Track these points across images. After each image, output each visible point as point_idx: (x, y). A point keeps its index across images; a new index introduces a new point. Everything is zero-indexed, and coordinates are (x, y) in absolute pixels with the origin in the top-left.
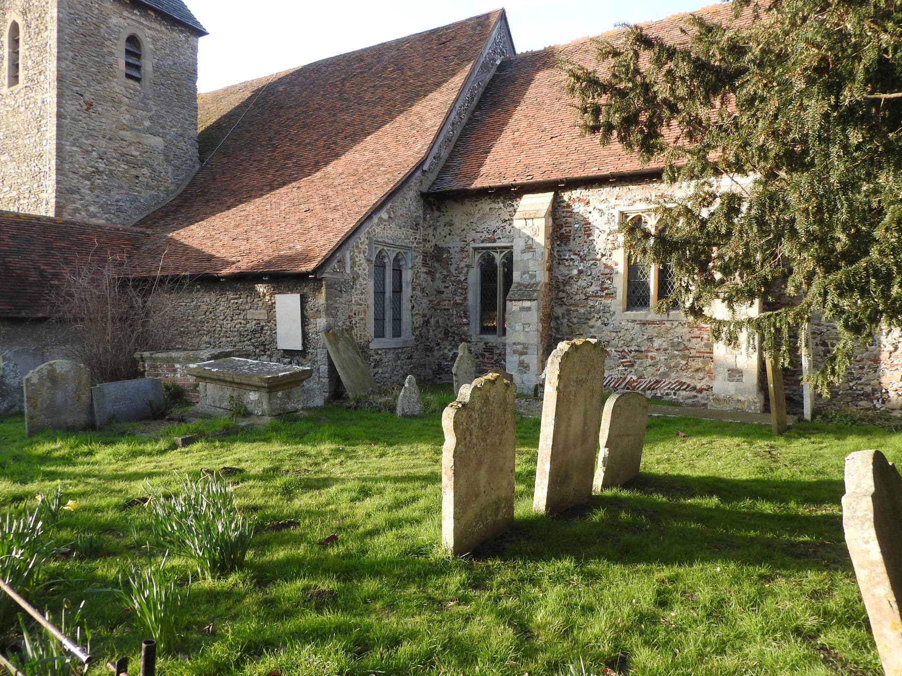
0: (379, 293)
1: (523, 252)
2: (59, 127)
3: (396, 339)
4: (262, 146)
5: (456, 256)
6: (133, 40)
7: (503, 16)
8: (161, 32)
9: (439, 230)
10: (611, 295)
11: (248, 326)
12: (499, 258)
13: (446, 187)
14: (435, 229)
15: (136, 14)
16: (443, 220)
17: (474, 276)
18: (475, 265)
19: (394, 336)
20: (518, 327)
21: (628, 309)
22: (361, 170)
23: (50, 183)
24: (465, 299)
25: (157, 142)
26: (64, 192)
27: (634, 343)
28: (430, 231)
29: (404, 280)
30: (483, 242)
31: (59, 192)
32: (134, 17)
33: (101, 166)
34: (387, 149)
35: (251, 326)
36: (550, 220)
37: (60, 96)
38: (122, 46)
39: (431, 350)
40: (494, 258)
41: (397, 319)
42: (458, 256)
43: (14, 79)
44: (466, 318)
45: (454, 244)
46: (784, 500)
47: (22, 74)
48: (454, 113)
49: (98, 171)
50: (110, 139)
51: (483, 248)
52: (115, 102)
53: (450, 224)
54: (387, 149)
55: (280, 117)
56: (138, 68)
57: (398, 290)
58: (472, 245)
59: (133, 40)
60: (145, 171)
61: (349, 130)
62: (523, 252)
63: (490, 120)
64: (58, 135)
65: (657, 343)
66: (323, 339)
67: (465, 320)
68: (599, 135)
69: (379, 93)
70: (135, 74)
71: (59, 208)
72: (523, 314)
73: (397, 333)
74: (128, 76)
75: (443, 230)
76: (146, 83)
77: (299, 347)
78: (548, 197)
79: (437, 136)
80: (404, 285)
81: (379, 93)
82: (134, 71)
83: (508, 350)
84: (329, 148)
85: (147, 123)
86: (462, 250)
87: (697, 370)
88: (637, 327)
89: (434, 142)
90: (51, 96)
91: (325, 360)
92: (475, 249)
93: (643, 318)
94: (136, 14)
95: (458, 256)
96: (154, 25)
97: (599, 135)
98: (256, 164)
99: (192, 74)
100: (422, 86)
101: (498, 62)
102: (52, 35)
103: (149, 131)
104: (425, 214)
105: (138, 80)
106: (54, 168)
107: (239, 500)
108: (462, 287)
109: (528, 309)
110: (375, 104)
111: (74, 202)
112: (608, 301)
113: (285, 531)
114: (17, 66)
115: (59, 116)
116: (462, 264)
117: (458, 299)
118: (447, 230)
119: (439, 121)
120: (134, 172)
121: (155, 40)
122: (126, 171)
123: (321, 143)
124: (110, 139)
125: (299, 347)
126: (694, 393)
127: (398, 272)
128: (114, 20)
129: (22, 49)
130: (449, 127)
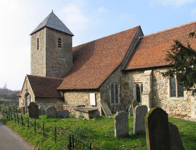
1: (145, 84)
2: (46, 58)
3: (116, 103)
4: (86, 59)
5: (130, 84)
6: (59, 39)
7: (140, 27)
9: (126, 78)
10: (166, 94)
11: (84, 100)
12: (140, 85)
13: (127, 69)
14: (125, 78)
16: (127, 76)
17: (135, 89)
18: (135, 86)
19: (116, 103)
20: (144, 101)
22: (108, 65)
23: (45, 70)
25: (64, 60)
26: (47, 72)
27: (173, 105)
28: (124, 79)
29: (118, 90)
30: (136, 81)
31: (47, 72)
33: (54, 66)
34: (113, 60)
35: (85, 100)
36: (151, 76)
37: (46, 52)
38: (58, 40)
39: (125, 106)
41: (117, 99)
42: (131, 84)
43: (38, 49)
45: (130, 82)
46: (71, 143)
47: (39, 48)
48: (129, 51)
49: (53, 67)
52: (57, 52)
53: (129, 77)
54: (113, 60)
56: (60, 45)
57: (117, 92)
58: (134, 82)
59: (59, 39)
60: (62, 66)
61: (105, 55)
62: (145, 84)
63: (137, 52)
64: (46, 60)
65: (178, 105)
66: (100, 103)
69: (112, 46)
70: (60, 46)
71: (47, 75)
72: (145, 98)
73: (117, 102)
74: (59, 46)
75: (127, 78)
76: (62, 47)
77: (95, 105)
78: (150, 71)
79: (125, 57)
80: (118, 91)
81: (112, 46)
82: (60, 46)
85: (62, 56)
86: (132, 83)
87: (189, 112)
88: (173, 101)
89: (124, 58)
90: (45, 52)
91: (101, 107)
92: (135, 83)
93: (175, 99)
95: (131, 84)
96: (63, 35)
99: (71, 44)
101: (139, 38)
102: (45, 40)
103: (63, 57)
104: (122, 75)
105: (60, 47)
106: (45, 66)
107: (105, 142)
108: (132, 91)
109: (146, 97)
110: (111, 49)
112: (166, 95)
113: (74, 146)
114: (38, 46)
115: (46, 56)
117: (131, 94)
118: (128, 78)
119: (125, 53)
120: (60, 66)
121: (64, 38)
122: (59, 66)
123: (99, 59)
125: (95, 105)
126: (188, 117)
127: (117, 88)
128: (56, 36)
129: (39, 43)
130: (127, 54)
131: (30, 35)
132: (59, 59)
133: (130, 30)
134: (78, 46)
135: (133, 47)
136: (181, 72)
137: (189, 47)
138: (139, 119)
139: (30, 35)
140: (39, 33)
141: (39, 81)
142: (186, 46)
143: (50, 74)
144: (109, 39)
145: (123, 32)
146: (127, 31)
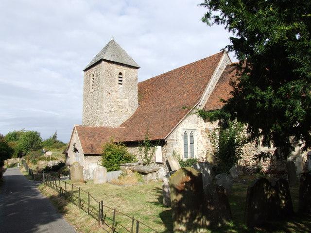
0: (186, 144)
25: (127, 101)
33: (112, 110)
38: (118, 76)
59: (120, 74)
60: (123, 109)
70: (121, 82)
123: (171, 97)
131: (84, 71)
132: (119, 100)
133: (214, 56)
134: (147, 81)
135: (216, 80)
136: (305, 193)
137: (224, 102)
138: (297, 83)
139: (84, 71)
140: (94, 69)
141: (91, 132)
142: (181, 159)
143: (106, 121)
144: (186, 69)
145: (205, 59)
146: (209, 57)
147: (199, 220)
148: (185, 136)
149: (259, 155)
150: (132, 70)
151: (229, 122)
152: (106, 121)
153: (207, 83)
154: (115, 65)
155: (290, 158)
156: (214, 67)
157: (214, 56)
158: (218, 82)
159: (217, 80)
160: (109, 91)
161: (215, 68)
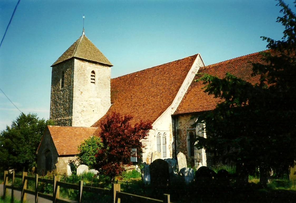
0: (159, 145)
4: (129, 99)
6: (93, 72)
8: (99, 68)
15: (94, 65)
21: (57, 181)
24: (186, 146)
25: (99, 100)
32: (93, 66)
33: (84, 109)
40: (193, 133)
44: (186, 151)
50: (87, 101)
51: (190, 130)
53: (181, 123)
55: (134, 88)
59: (93, 72)
60: (96, 109)
67: (186, 152)
68: (65, 195)
83: (195, 161)
84: (147, 100)
94: (94, 65)
97: (65, 195)
98: (127, 105)
100: (174, 80)
111: (77, 120)
116: (184, 135)
124: (87, 101)
144: (160, 70)
147: (229, 150)
148: (159, 137)
149: (287, 41)
150: (105, 68)
151: (179, 83)
152: (78, 121)
153: (179, 87)
154: (87, 63)
155: (78, 185)
156: (187, 70)
157: (187, 58)
158: (191, 85)
159: (190, 84)
160: (81, 90)
161: (188, 71)
